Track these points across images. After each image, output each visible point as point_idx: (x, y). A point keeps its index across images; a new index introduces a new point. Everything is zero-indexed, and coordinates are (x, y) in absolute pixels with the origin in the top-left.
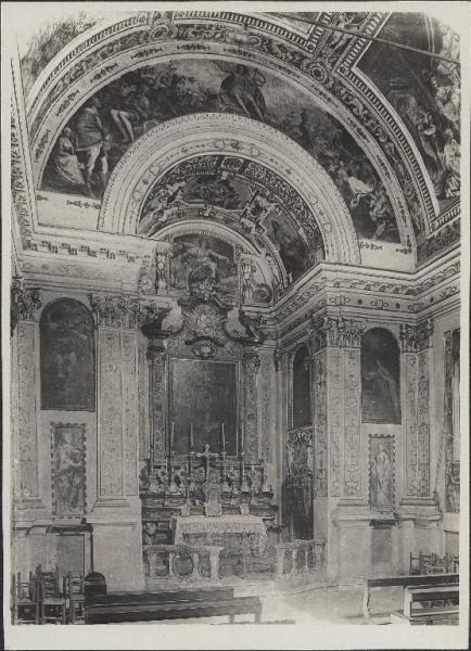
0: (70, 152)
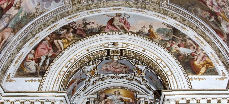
0: (32, 60)
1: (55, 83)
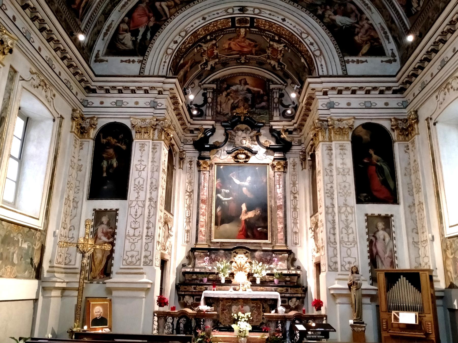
1: (160, 64)
